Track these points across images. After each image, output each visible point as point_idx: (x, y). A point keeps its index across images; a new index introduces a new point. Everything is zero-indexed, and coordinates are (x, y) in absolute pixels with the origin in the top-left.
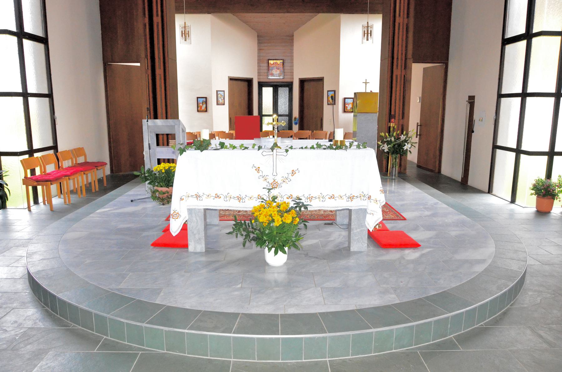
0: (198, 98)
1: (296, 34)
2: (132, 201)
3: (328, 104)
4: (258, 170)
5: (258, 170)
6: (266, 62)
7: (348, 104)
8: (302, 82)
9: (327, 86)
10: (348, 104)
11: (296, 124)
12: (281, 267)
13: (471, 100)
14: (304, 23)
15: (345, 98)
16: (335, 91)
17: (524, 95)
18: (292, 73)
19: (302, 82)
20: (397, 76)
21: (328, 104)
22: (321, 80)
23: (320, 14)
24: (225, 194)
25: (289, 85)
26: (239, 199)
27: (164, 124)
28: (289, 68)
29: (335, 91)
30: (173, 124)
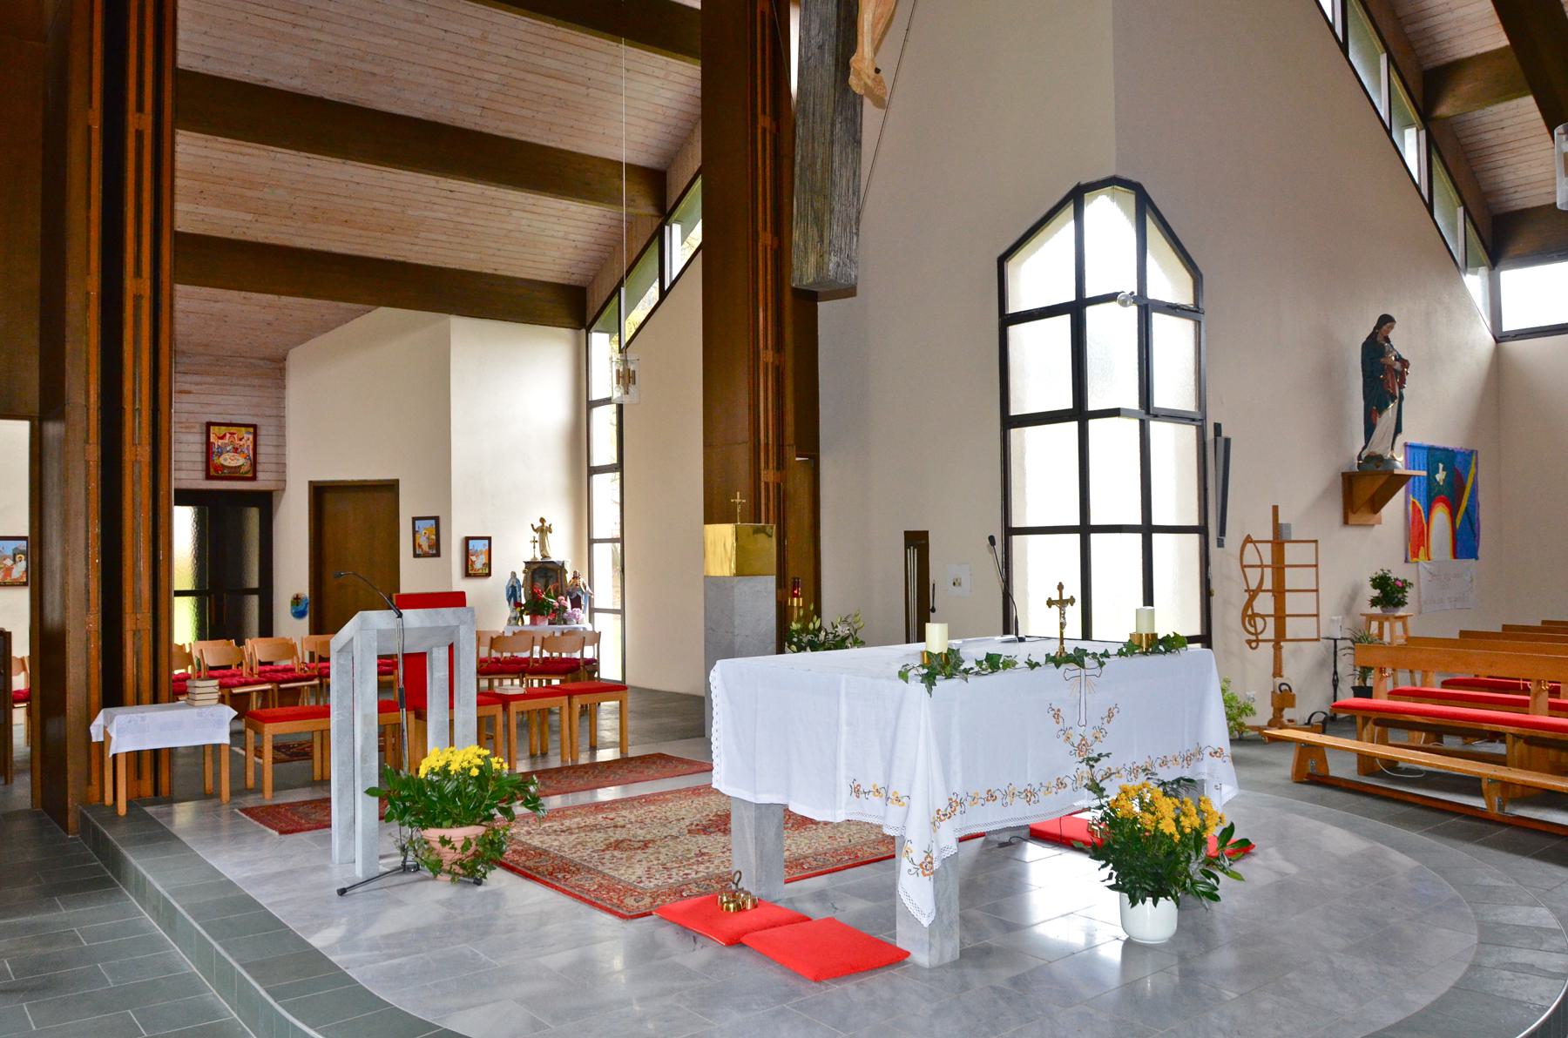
0: (489, 539)
1: (295, 357)
2: (342, 892)
3: (416, 556)
4: (1057, 716)
5: (1057, 716)
6: (199, 429)
7: (476, 554)
8: (319, 492)
9: (408, 509)
10: (476, 554)
11: (299, 615)
12: (1166, 945)
13: (917, 541)
14: (326, 328)
15: (467, 539)
16: (437, 519)
17: (1085, 529)
18: (281, 467)
19: (319, 492)
20: (767, 484)
21: (416, 556)
22: (390, 488)
23: (382, 309)
24: (1004, 787)
25: (266, 502)
26: (1029, 795)
27: (428, 624)
28: (270, 450)
29: (437, 519)
30: (454, 623)
